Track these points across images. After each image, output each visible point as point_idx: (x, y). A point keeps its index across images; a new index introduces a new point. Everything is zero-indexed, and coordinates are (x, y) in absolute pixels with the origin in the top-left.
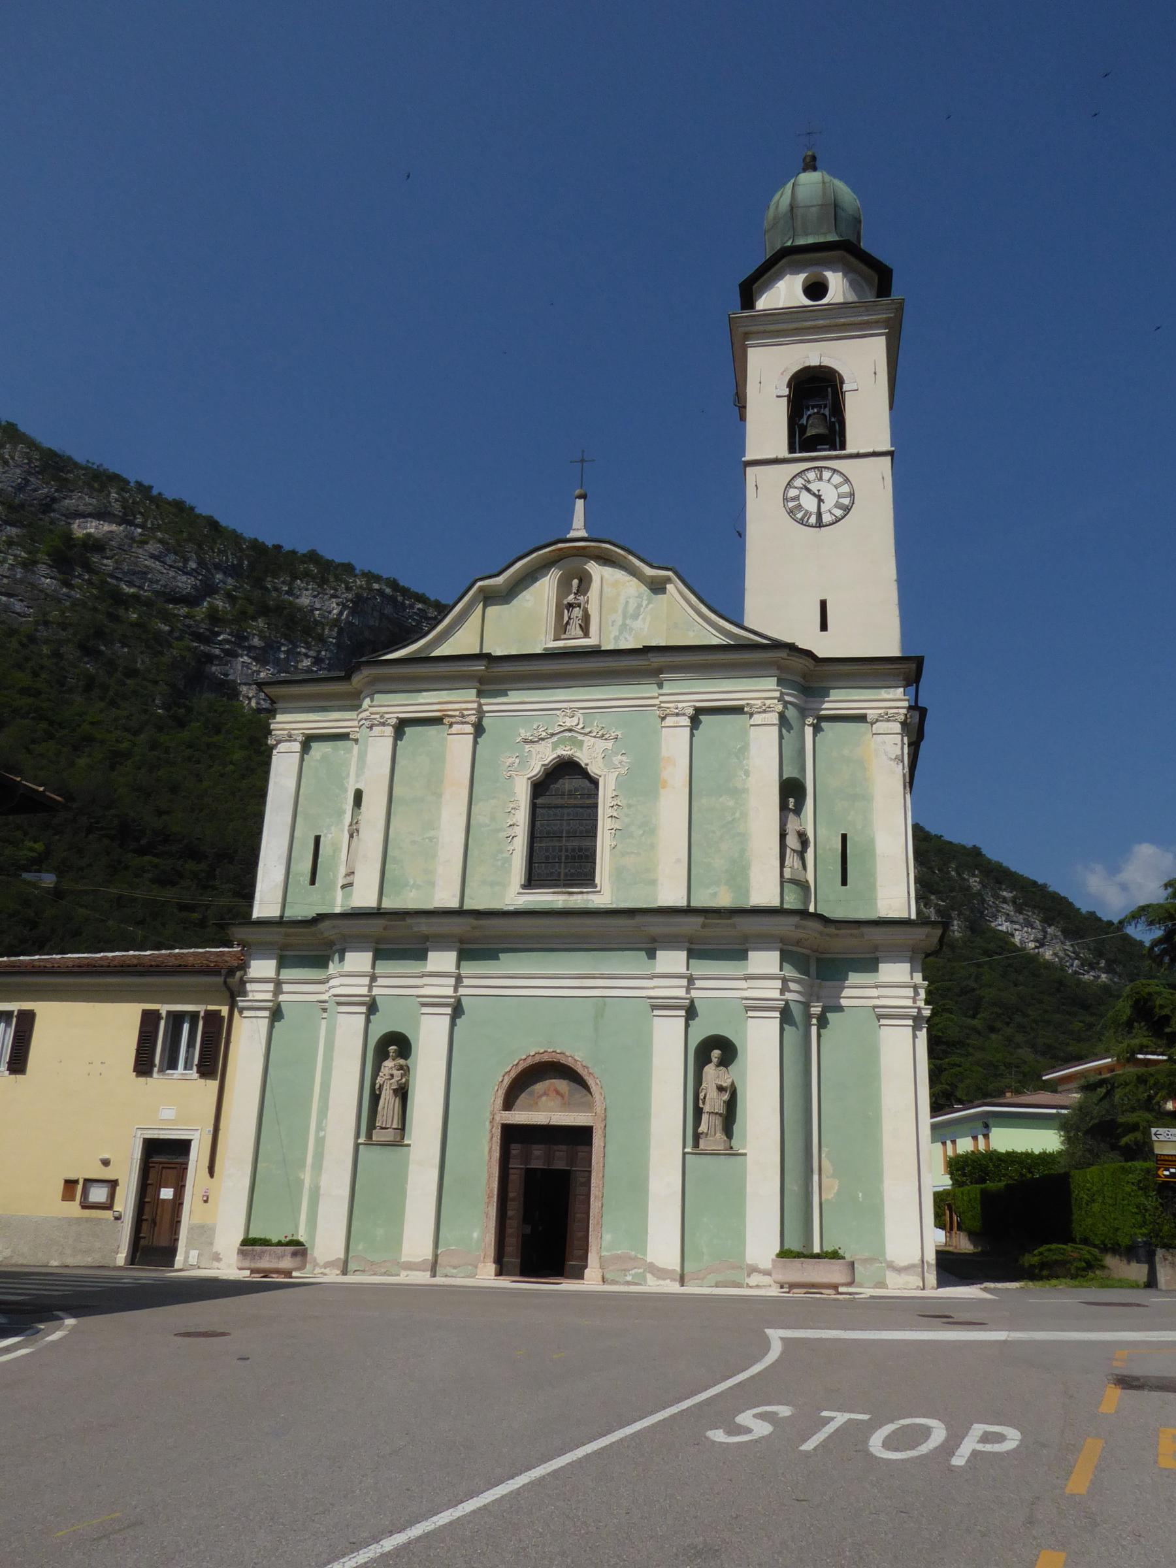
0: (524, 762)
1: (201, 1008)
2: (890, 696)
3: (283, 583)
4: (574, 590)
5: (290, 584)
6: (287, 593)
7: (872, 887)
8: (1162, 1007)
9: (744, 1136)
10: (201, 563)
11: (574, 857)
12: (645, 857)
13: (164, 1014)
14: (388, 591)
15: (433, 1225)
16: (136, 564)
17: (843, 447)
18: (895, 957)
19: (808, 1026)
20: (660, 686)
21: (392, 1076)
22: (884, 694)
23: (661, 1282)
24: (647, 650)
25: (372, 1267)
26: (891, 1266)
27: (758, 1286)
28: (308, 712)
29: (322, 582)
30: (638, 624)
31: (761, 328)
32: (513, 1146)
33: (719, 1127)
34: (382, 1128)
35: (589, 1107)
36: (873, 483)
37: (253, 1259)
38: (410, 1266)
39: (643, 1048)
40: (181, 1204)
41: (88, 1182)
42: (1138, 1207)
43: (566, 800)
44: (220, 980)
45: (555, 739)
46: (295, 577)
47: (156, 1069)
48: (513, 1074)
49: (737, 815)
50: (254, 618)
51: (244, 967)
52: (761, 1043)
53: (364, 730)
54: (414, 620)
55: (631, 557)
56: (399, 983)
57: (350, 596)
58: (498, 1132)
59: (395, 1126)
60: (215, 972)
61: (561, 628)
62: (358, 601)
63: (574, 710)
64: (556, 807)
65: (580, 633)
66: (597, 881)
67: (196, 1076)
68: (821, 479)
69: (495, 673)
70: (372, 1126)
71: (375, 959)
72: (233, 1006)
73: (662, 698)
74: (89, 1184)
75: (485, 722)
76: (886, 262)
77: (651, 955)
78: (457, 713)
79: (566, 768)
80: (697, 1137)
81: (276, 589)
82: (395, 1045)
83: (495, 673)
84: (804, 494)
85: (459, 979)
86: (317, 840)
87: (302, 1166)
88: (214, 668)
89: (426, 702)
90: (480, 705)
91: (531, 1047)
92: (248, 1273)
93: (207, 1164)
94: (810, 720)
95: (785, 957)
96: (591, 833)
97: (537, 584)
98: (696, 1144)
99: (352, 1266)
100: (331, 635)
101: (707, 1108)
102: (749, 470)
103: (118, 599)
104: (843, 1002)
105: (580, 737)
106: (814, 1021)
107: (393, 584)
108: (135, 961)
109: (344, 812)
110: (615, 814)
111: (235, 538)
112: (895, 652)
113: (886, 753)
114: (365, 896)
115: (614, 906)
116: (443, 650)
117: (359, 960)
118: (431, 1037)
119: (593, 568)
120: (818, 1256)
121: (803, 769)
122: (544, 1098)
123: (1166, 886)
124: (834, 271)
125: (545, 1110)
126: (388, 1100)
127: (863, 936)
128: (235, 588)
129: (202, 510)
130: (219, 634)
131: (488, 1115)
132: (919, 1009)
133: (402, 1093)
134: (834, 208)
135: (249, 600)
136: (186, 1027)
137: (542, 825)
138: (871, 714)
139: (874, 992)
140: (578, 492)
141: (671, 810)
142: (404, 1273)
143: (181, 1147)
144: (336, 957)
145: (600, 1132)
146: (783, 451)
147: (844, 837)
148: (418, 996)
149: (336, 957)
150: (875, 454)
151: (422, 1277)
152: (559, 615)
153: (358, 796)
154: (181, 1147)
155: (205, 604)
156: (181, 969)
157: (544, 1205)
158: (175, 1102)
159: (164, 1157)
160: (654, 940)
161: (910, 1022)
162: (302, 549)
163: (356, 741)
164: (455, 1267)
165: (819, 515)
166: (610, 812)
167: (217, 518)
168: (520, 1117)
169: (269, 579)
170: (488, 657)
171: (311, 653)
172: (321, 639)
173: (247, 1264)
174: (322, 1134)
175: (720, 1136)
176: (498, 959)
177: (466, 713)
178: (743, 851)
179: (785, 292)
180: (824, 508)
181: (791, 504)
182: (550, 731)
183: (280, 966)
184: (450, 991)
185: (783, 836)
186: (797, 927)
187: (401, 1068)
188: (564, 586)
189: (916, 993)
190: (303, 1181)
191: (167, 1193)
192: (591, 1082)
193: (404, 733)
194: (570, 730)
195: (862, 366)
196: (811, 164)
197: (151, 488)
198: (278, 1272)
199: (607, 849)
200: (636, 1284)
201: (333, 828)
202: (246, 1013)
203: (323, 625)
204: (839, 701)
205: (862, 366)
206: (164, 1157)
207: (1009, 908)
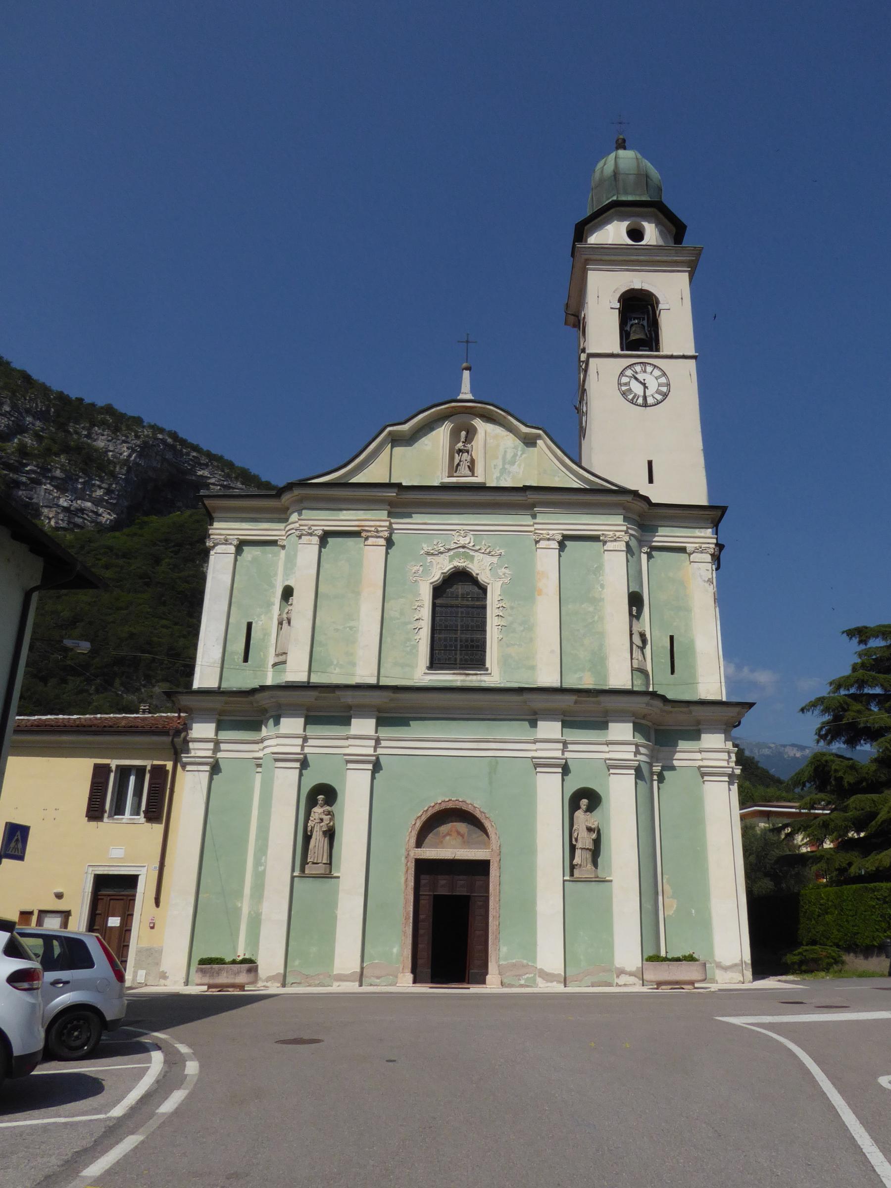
0: (427, 570)
1: (148, 763)
2: (702, 535)
3: (83, 428)
4: (463, 439)
5: (89, 429)
6: (86, 436)
8: (836, 771)
9: (610, 866)
10: (14, 407)
11: (467, 646)
12: (525, 647)
13: (114, 768)
14: (170, 440)
15: (360, 943)
17: (658, 350)
18: (713, 729)
19: (652, 780)
20: (534, 516)
21: (322, 820)
22: (697, 532)
23: (549, 984)
24: (526, 489)
25: (307, 980)
26: (719, 966)
27: (625, 985)
28: (242, 521)
29: (116, 430)
30: (514, 469)
31: (599, 257)
32: (422, 877)
33: (590, 860)
34: (314, 863)
35: (486, 845)
36: (684, 378)
37: (212, 976)
38: (341, 978)
39: (527, 800)
40: (129, 931)
41: (43, 913)
42: (881, 916)
43: (458, 602)
44: (167, 739)
45: (452, 553)
47: (106, 815)
48: (424, 818)
49: (596, 618)
50: (57, 455)
51: (186, 728)
52: (621, 793)
53: (293, 538)
54: (189, 464)
55: (510, 418)
56: (325, 743)
57: (138, 442)
58: (412, 865)
59: (324, 861)
60: (165, 733)
61: (453, 469)
62: (145, 446)
63: (467, 532)
64: (452, 606)
65: (469, 473)
66: (488, 665)
68: (645, 372)
69: (403, 499)
70: (304, 862)
71: (306, 724)
72: (176, 760)
73: (536, 526)
74: (43, 915)
75: (394, 537)
76: (683, 220)
77: (533, 724)
78: (373, 529)
79: (460, 578)
80: (572, 867)
81: (77, 433)
82: (324, 794)
83: (403, 499)
84: (633, 382)
85: (378, 741)
86: (249, 625)
87: (239, 894)
88: (20, 493)
89: (347, 519)
90: (391, 524)
91: (439, 797)
92: (205, 988)
93: (154, 895)
94: (645, 549)
95: (637, 728)
96: (481, 627)
97: (434, 433)
99: (289, 980)
100: (121, 472)
101: (579, 845)
102: (591, 360)
104: (676, 763)
105: (472, 553)
106: (655, 777)
107: (174, 435)
108: (89, 723)
109: (273, 604)
110: (501, 614)
111: (45, 390)
112: (704, 502)
113: (701, 576)
114: (296, 672)
115: (502, 685)
116: (354, 480)
117: (292, 725)
118: (355, 788)
119: (478, 423)
120: (666, 959)
122: (448, 838)
123: (831, 684)
124: (649, 222)
125: (450, 847)
126: (318, 841)
127: (691, 712)
128: (43, 430)
129: (17, 364)
130: (27, 465)
131: (403, 852)
132: (733, 768)
133: (330, 834)
134: (644, 178)
135: (54, 441)
136: (132, 779)
137: (441, 620)
138: (690, 547)
139: (698, 756)
140: (465, 365)
141: (546, 612)
142: (336, 984)
143: (131, 881)
144: (271, 722)
145: (496, 865)
146: (617, 350)
147: (672, 638)
148: (345, 755)
149: (271, 722)
150: (684, 357)
151: (352, 987)
152: (452, 458)
153: (288, 593)
154: (131, 881)
155: (16, 440)
156: (132, 730)
157: (450, 925)
158: (124, 844)
159: (113, 891)
160: (535, 713)
161: (726, 779)
162: (100, 402)
163: (283, 547)
164: (378, 978)
165: (645, 398)
166: (497, 612)
167: (30, 372)
168: (429, 853)
169: (71, 424)
170: (399, 486)
171: (104, 485)
172: (113, 475)
173: (206, 980)
174: (261, 869)
175: (590, 866)
176: (409, 725)
177: (380, 529)
178: (601, 646)
179: (613, 233)
180: (648, 393)
181: (624, 388)
182: (448, 547)
183: (218, 729)
184: (370, 751)
185: (631, 635)
186: (647, 704)
187: (329, 813)
188: (455, 435)
189: (730, 757)
190: (240, 909)
191: (114, 922)
192: (487, 824)
193: (327, 542)
194: (463, 547)
195: (672, 291)
196: (622, 145)
198: (233, 986)
199: (495, 641)
200: (528, 986)
201: (263, 617)
202: (189, 768)
203: (115, 464)
204: (665, 536)
205: (672, 291)
206: (113, 891)
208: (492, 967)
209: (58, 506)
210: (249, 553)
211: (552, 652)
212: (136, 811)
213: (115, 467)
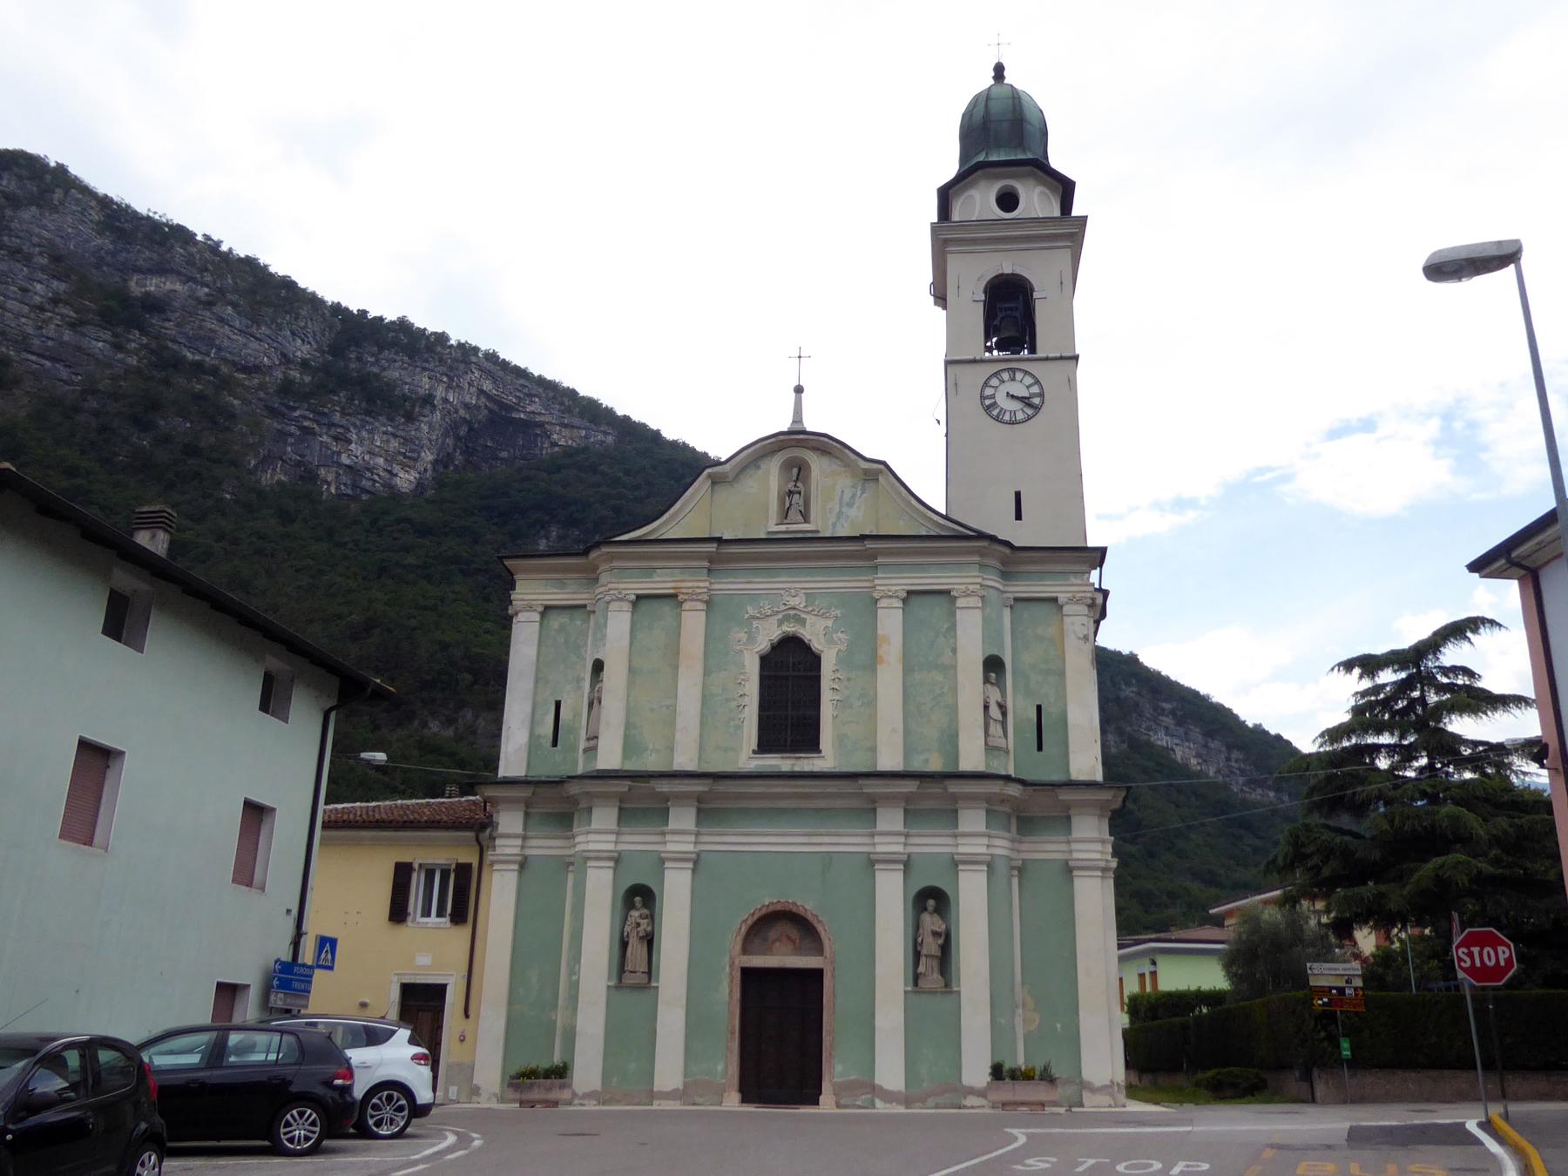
0: (751, 638)
7: (1065, 756)
12: (869, 721)
16: (201, 328)
24: (863, 538)
44: (471, 834)
46: (381, 349)
48: (750, 922)
61: (785, 514)
67: (449, 924)
68: (1013, 379)
69: (721, 553)
80: (916, 978)
91: (767, 899)
98: (916, 984)
101: (924, 952)
103: (177, 363)
114: (610, 757)
118: (676, 891)
121: (1002, 647)
126: (636, 950)
130: (295, 409)
131: (727, 959)
133: (650, 941)
138: (1062, 598)
141: (889, 683)
143: (439, 991)
147: (1039, 708)
153: (598, 666)
154: (439, 991)
158: (429, 949)
170: (719, 540)
173: (518, 1096)
175: (936, 975)
181: (988, 402)
197: (218, 243)
207: (1168, 721)
208: (826, 1086)
209: (340, 465)
210: (556, 621)
211: (894, 730)
212: (440, 914)
213: (413, 407)
